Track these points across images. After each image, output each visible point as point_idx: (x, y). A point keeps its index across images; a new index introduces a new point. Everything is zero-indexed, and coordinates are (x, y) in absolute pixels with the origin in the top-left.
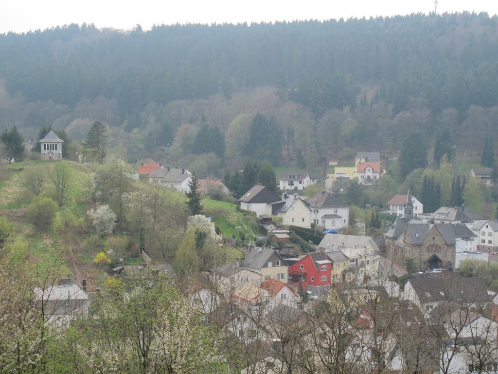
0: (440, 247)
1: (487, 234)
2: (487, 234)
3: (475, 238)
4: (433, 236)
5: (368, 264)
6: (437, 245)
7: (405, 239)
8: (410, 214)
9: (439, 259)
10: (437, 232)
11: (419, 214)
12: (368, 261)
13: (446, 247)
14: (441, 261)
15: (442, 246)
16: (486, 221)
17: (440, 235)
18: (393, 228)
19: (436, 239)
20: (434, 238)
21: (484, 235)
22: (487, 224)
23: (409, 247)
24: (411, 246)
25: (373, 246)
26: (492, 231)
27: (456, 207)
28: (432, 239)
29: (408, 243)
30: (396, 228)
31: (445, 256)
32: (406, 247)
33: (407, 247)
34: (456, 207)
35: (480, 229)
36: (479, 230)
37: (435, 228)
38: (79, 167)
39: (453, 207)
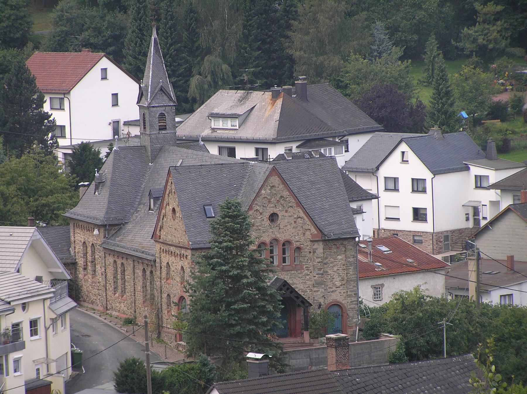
0: (299, 248)
1: (405, 185)
2: (405, 185)
3: (366, 206)
4: (270, 210)
5: (34, 332)
6: (288, 242)
7: (158, 227)
8: (163, 128)
9: (298, 296)
10: (286, 193)
11: (127, 124)
12: (33, 323)
13: (320, 247)
14: (305, 303)
15: (307, 246)
16: (399, 136)
17: (299, 204)
18: (100, 185)
19: (282, 221)
20: (273, 217)
21: (396, 189)
22: (404, 147)
23: (182, 256)
24: (189, 253)
25: (45, 262)
26: (423, 173)
27: (276, 88)
28: (267, 222)
29: (175, 241)
30: (114, 183)
31: (318, 284)
32: (166, 259)
33: (172, 259)
34: (276, 88)
35: (378, 168)
36: (373, 172)
37: (275, 180)
38: (199, 384)
39: (265, 87)
